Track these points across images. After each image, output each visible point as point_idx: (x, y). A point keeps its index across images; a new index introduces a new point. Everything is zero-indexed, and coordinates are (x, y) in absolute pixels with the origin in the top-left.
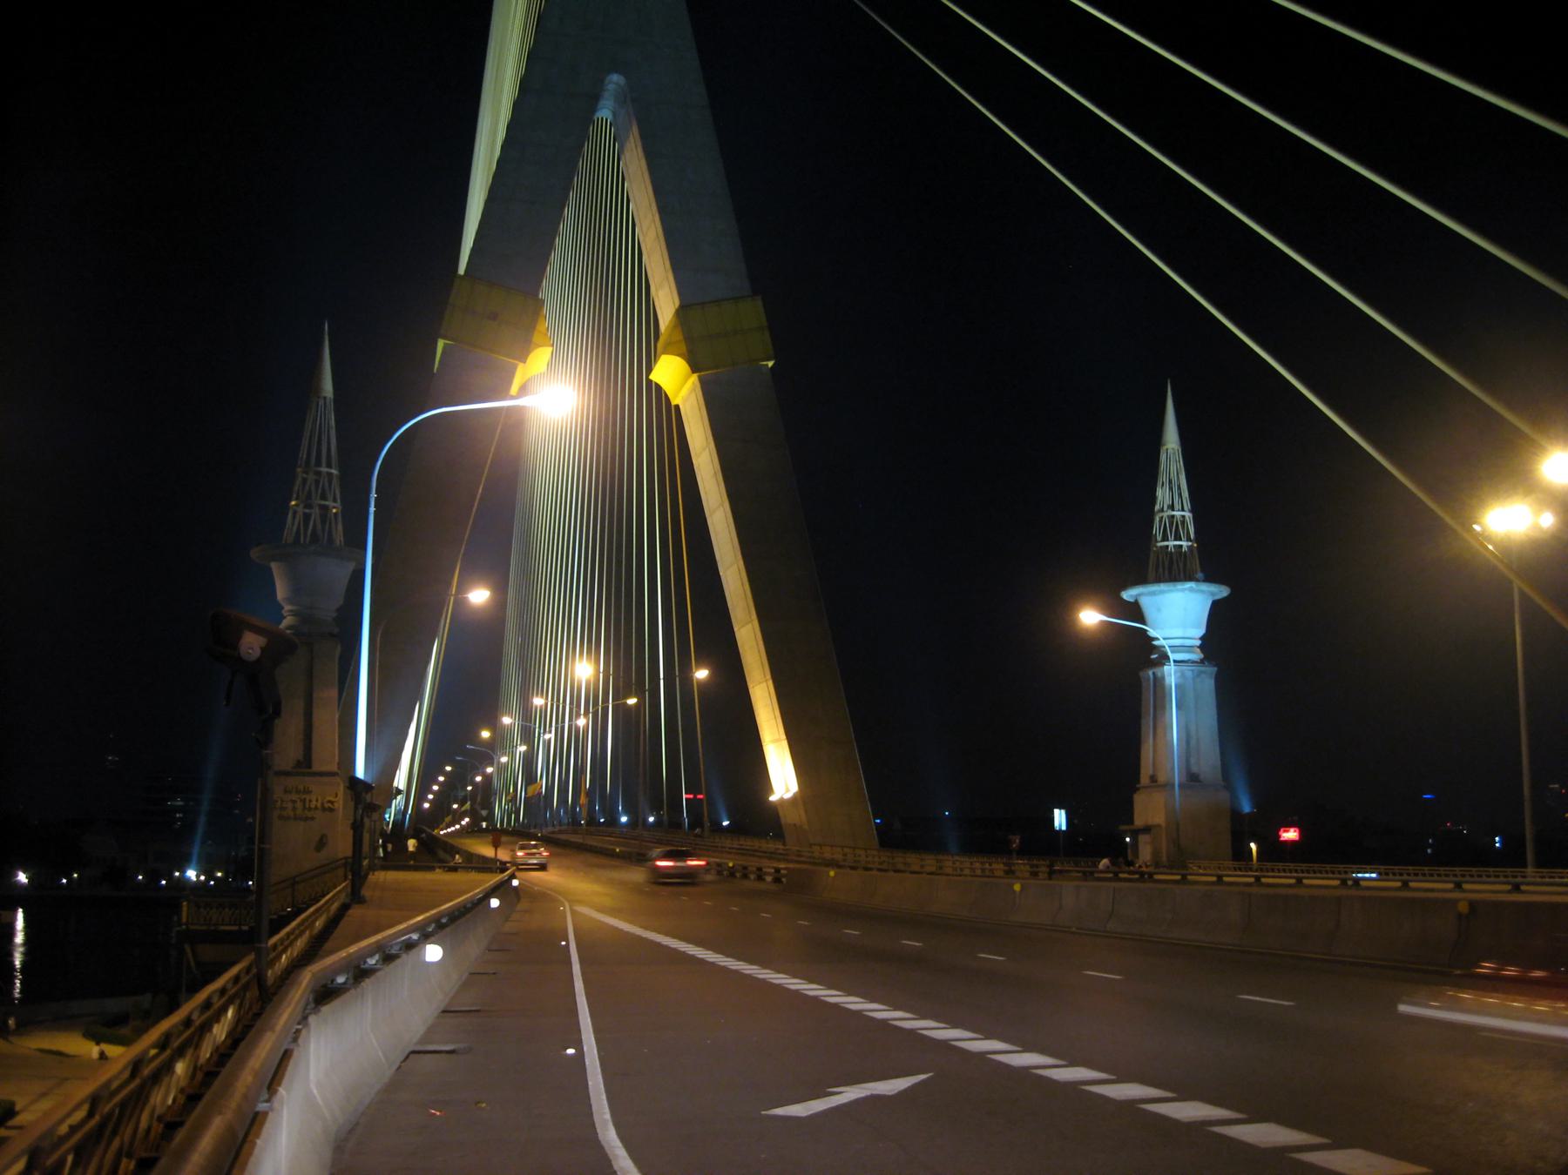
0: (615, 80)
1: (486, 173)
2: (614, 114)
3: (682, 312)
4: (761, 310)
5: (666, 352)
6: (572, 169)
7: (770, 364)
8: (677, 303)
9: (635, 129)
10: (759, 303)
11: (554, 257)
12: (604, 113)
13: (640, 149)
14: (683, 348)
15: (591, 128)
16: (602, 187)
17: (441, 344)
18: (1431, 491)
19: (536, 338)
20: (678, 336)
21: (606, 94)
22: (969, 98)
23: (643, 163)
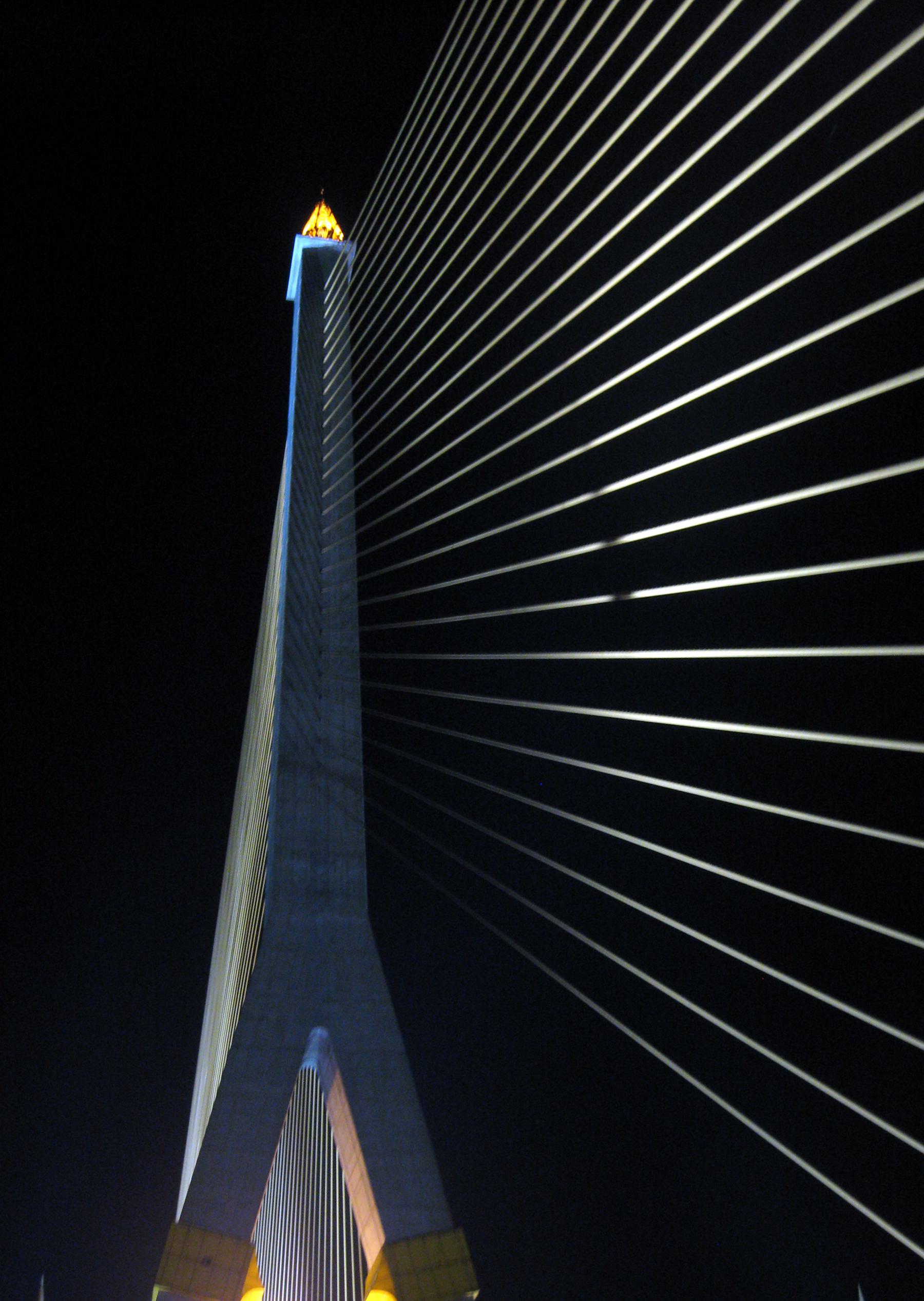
0: (319, 1033)
1: (203, 1116)
2: (319, 1063)
3: (388, 1249)
4: (463, 1242)
5: (374, 1287)
6: (282, 1110)
7: (475, 1294)
8: (383, 1241)
9: (338, 1072)
10: (461, 1234)
11: (268, 1191)
12: (310, 1063)
13: (343, 1095)
14: (390, 1284)
15: (295, 1088)
16: (304, 1178)
17: (156, 1291)
18: (340, 253)
19: (248, 1281)
20: (385, 1272)
21: (311, 1047)
22: (408, 393)
23: (347, 1108)
